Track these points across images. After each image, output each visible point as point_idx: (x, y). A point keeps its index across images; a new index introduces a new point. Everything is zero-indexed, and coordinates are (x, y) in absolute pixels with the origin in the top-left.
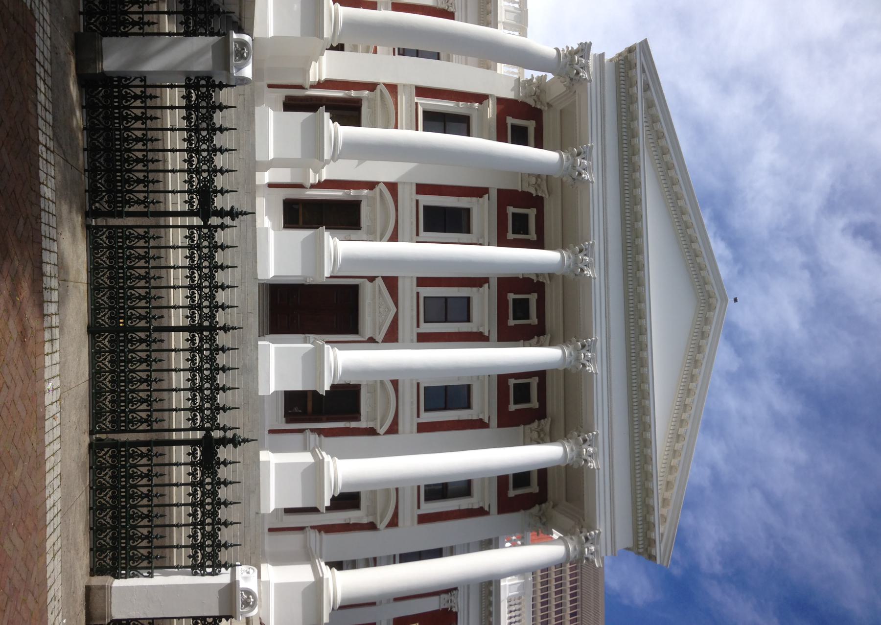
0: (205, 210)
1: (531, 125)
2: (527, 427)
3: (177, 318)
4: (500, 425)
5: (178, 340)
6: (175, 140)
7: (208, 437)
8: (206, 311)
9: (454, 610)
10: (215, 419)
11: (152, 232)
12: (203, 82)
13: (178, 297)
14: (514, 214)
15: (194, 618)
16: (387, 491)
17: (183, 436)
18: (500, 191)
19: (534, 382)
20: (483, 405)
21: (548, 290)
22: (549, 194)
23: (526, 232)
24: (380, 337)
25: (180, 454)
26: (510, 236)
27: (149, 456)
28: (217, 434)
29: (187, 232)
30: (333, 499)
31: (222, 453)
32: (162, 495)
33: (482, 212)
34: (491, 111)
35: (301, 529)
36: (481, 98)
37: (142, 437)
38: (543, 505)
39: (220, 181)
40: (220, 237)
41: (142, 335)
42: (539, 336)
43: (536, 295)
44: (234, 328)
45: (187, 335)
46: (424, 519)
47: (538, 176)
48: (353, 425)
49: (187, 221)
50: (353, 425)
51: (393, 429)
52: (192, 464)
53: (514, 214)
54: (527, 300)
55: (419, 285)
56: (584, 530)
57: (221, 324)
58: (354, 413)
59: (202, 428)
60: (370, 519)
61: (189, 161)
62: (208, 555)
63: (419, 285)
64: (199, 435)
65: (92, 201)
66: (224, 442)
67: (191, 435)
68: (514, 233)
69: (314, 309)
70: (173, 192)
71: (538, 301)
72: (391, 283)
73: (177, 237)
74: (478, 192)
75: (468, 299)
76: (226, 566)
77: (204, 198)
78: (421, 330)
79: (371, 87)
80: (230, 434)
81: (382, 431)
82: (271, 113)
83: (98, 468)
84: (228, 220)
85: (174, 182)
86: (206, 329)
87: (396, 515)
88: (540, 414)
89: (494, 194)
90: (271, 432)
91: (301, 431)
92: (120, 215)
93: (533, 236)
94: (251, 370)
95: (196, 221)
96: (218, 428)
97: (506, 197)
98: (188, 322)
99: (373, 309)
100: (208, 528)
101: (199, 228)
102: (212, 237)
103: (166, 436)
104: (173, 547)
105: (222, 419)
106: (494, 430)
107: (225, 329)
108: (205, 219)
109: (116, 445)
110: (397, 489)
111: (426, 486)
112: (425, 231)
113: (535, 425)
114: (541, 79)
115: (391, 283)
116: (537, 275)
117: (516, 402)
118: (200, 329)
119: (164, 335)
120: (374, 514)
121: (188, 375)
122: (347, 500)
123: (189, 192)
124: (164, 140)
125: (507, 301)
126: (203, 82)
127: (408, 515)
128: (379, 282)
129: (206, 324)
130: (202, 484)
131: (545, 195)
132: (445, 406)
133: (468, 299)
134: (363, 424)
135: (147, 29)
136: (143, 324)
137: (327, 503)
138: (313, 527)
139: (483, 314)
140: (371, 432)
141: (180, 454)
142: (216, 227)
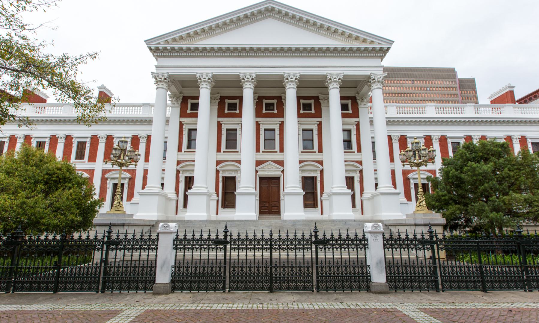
0: (224, 242)
1: (190, 102)
2: (322, 105)
3: (267, 255)
4: (320, 116)
5: (276, 255)
6: (196, 255)
7: (227, 242)
9: (520, 137)
12: (175, 242)
13: (258, 255)
14: (191, 110)
15: (384, 249)
16: (346, 165)
17: (314, 253)
18: (181, 116)
19: (302, 101)
20: (312, 123)
21: (222, 95)
22: (218, 93)
23: (236, 104)
24: (282, 168)
26: (237, 111)
27: (322, 267)
28: (313, 239)
30: (349, 188)
31: (320, 236)
33: (228, 123)
34: (186, 120)
35: (362, 201)
36: (181, 125)
37: (315, 271)
38: (357, 98)
39: (213, 236)
40: (235, 237)
41: (274, 270)
43: (226, 100)
44: (271, 231)
46: (359, 150)
47: (211, 98)
48: (319, 179)
50: (319, 179)
52: (325, 249)
53: (191, 110)
54: (266, 104)
55: (220, 152)
56: (370, 80)
57: (269, 237)
58: (313, 179)
59: (311, 245)
60: (358, 172)
62: (361, 243)
63: (220, 152)
64: (314, 246)
66: (316, 236)
67: (314, 249)
70: (333, 256)
72: (259, 163)
73: (234, 254)
74: (219, 125)
75: (227, 130)
76: (364, 236)
77: (220, 243)
78: (278, 151)
80: (313, 234)
81: (282, 168)
84: (229, 234)
85: (353, 255)
86: (271, 242)
87: (357, 162)
88: (317, 99)
89: (220, 119)
90: (322, 214)
91: (321, 202)
92: (225, 278)
93: (237, 101)
94: (294, 223)
95: (228, 246)
96: (311, 238)
97: (221, 114)
98: (269, 251)
100: (350, 242)
101: (231, 245)
102: (235, 240)
103: (314, 261)
104: (333, 258)
105: (307, 237)
106: (323, 119)
107: (271, 235)
108: (227, 242)
109: (318, 281)
110: (345, 161)
111: (345, 149)
114: (170, 97)
115: (259, 163)
116: (254, 99)
118: (271, 245)
119: (274, 261)
120: (356, 171)
121: (351, 250)
122: (350, 182)
124: (308, 259)
125: (228, 113)
126: (175, 242)
127: (356, 157)
128: (258, 168)
129: (269, 243)
131: (219, 95)
133: (227, 130)
134: (318, 175)
135: (153, 265)
136: (269, 269)
137: (350, 191)
138: (361, 196)
139: (272, 123)
140: (322, 172)
141: (321, 254)
142: (231, 238)
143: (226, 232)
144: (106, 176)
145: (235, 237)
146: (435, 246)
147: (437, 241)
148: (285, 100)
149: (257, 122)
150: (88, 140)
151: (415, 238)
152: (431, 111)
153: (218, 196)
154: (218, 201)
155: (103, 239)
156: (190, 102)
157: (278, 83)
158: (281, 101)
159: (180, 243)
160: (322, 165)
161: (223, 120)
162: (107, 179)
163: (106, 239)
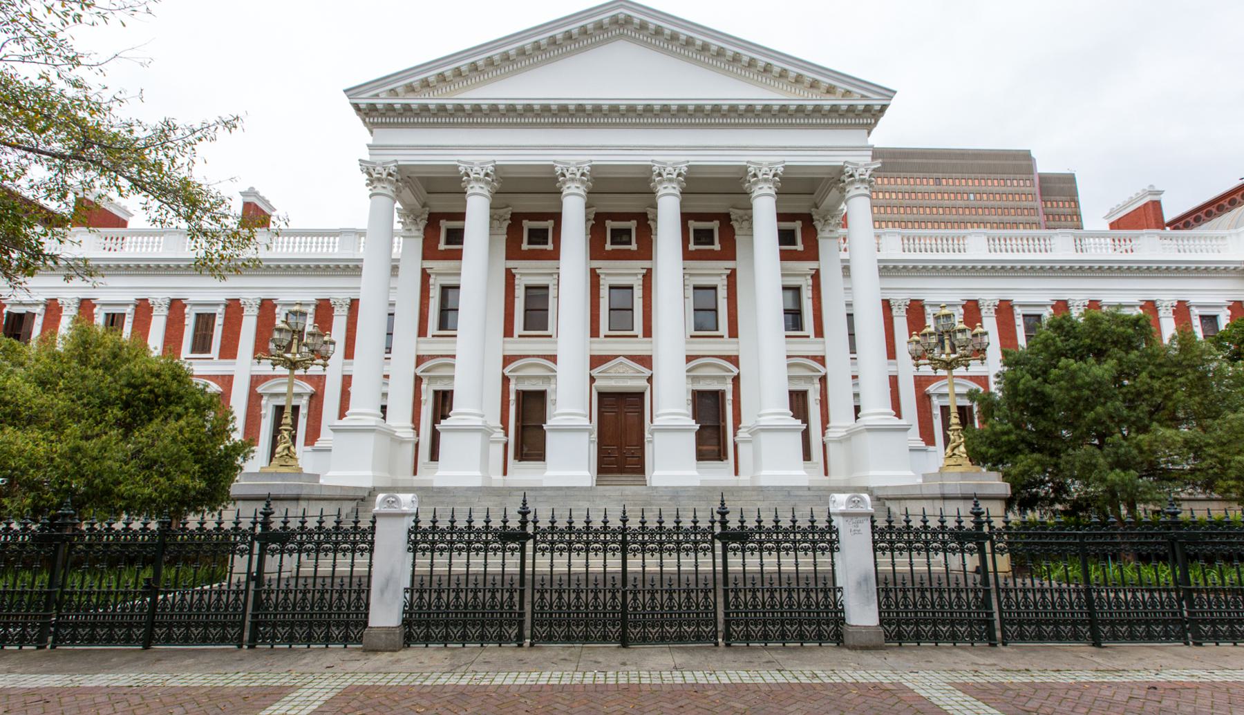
0: (520, 537)
1: (445, 225)
2: (737, 232)
7: (721, 537)
8: (573, 537)
9: (1175, 304)
10: (670, 530)
11: (538, 587)
12: (412, 537)
15: (875, 550)
16: (789, 366)
17: (719, 561)
19: (693, 225)
20: (713, 273)
22: (507, 206)
23: (546, 231)
24: (647, 373)
25: (735, 563)
26: (550, 247)
27: (736, 591)
28: (718, 530)
29: (539, 554)
30: (796, 416)
31: (733, 523)
32: (807, 579)
33: (529, 273)
34: (435, 265)
35: (824, 446)
36: (425, 276)
37: (720, 600)
39: (496, 523)
40: (544, 524)
41: (630, 597)
42: (730, 220)
44: (624, 512)
45: (630, 556)
46: (819, 332)
48: (729, 397)
49: (529, 553)
50: (729, 397)
51: (734, 360)
52: (743, 551)
53: (448, 243)
54: (695, 231)
55: (425, 335)
57: (620, 524)
58: (718, 396)
59: (713, 543)
60: (817, 381)
61: (478, 550)
62: (823, 538)
63: (425, 335)
64: (718, 545)
65: (509, 640)
66: (724, 523)
67: (719, 552)
68: (546, 243)
69: (621, 431)
71: (696, 220)
72: (596, 361)
73: (543, 564)
74: (510, 277)
75: (527, 288)
76: (830, 521)
77: (511, 538)
79: (506, 380)
80: (718, 517)
81: (647, 373)
82: (439, 473)
83: (501, 638)
84: (530, 517)
86: (624, 537)
87: (814, 358)
88: (725, 219)
92: (522, 615)
93: (549, 224)
94: (676, 493)
95: (529, 545)
96: (712, 527)
97: (513, 252)
99: (622, 379)
100: (799, 537)
101: (535, 542)
103: (720, 577)
105: (704, 524)
106: (739, 264)
107: (624, 520)
108: (527, 537)
109: (727, 623)
110: (788, 357)
112: (546, 329)
113: (735, 225)
114: (401, 215)
115: (596, 361)
116: (587, 220)
117: (794, 243)
118: (624, 543)
119: (630, 578)
120: (811, 378)
122: (798, 402)
123: (504, 551)
127: (812, 347)
128: (595, 373)
129: (620, 537)
130: (760, 542)
132: (713, 312)
133: (527, 288)
134: (728, 387)
135: (364, 587)
136: (619, 595)
137: (799, 422)
139: (626, 272)
140: (736, 380)
142: (535, 528)
143: (267, 515)
144: (259, 390)
145: (544, 524)
146: (988, 545)
147: (991, 534)
148: (655, 220)
149: (593, 271)
150: (220, 310)
151: (943, 527)
152: (977, 246)
153: (507, 435)
154: (506, 446)
155: (253, 529)
156: (445, 225)
157: (641, 184)
158: (645, 223)
159: (422, 539)
160: (823, 364)
161: (519, 266)
162: (261, 396)
163: (259, 529)
